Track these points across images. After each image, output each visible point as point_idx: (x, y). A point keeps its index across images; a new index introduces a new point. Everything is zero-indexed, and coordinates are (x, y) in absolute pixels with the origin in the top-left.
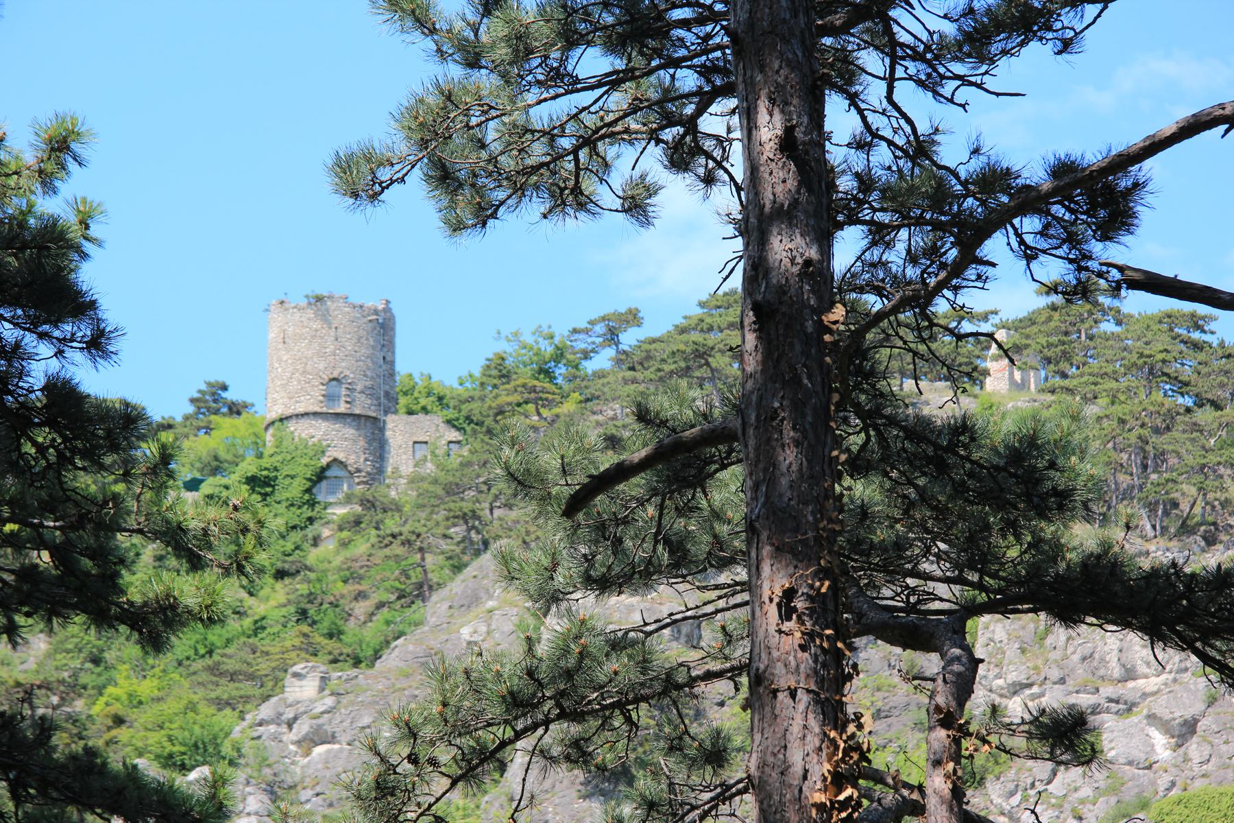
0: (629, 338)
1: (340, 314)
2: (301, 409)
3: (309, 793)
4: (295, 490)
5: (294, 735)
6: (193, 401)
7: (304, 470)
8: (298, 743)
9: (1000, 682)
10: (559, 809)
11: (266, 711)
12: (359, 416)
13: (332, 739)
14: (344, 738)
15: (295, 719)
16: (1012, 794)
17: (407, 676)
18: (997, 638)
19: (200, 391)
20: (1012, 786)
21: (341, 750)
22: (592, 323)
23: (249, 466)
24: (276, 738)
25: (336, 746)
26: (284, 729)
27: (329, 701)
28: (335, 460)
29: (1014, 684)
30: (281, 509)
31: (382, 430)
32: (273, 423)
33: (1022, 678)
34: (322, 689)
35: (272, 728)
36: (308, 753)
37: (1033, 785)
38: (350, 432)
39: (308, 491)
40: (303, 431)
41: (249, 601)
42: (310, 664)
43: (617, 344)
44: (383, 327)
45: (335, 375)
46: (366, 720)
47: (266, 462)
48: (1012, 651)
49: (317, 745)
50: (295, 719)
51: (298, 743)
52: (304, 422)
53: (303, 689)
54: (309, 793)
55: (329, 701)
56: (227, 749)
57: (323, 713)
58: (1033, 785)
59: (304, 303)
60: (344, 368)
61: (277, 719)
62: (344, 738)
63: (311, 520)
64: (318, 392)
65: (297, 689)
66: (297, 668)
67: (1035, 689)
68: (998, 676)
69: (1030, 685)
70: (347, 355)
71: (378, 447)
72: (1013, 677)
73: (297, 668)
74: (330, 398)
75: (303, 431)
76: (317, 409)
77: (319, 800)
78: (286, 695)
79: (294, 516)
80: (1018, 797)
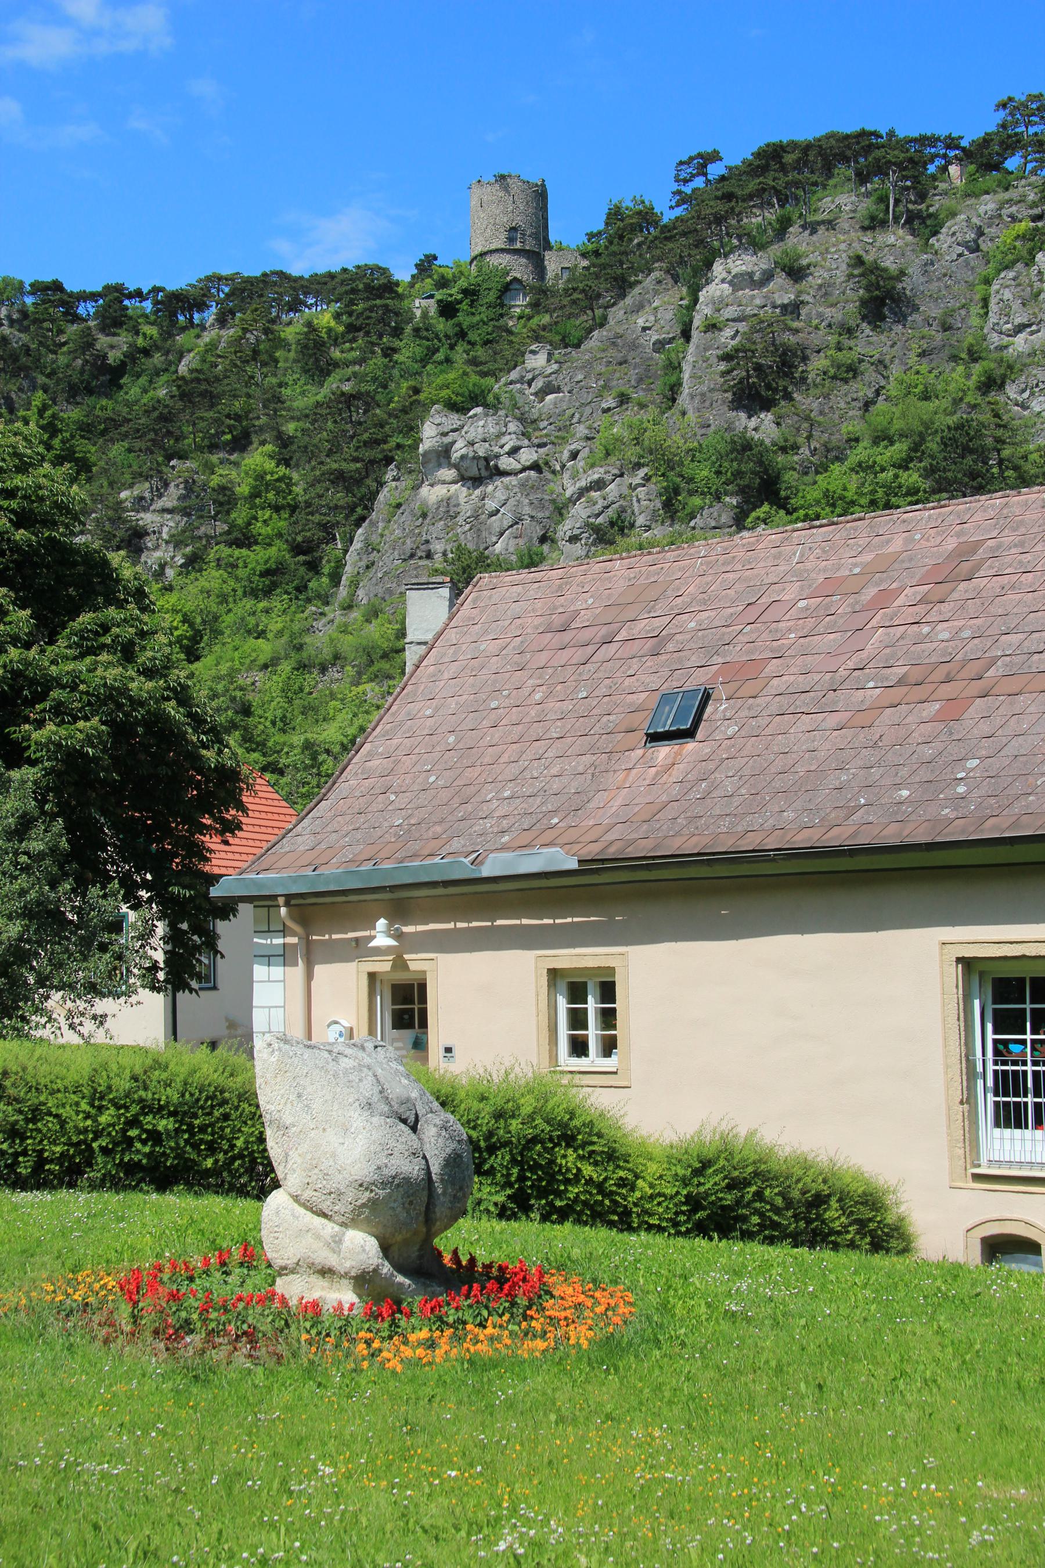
0: (715, 170)
1: (515, 186)
2: (493, 247)
3: (546, 423)
4: (492, 297)
5: (532, 390)
7: (495, 284)
8: (536, 394)
9: (1009, 326)
11: (514, 375)
13: (558, 390)
14: (566, 389)
15: (533, 379)
16: (1023, 391)
17: (604, 351)
18: (1005, 298)
20: (1023, 386)
22: (691, 159)
23: (463, 283)
24: (521, 392)
26: (526, 386)
27: (555, 367)
29: (1020, 325)
30: (483, 309)
31: (543, 260)
32: (475, 258)
33: (1025, 321)
34: (549, 361)
35: (518, 386)
36: (542, 400)
37: (1037, 385)
38: (523, 261)
39: (499, 297)
40: (494, 260)
41: (335, 635)
43: (705, 175)
44: (540, 196)
46: (580, 377)
47: (473, 281)
48: (1016, 305)
50: (533, 379)
51: (536, 394)
52: (497, 255)
53: (537, 361)
54: (546, 423)
55: (555, 367)
56: (490, 398)
58: (1037, 385)
59: (493, 180)
60: (518, 220)
61: (521, 380)
62: (566, 389)
63: (502, 316)
64: (503, 236)
67: (1034, 328)
68: (1007, 323)
69: (1030, 326)
70: (520, 215)
71: (540, 269)
72: (1018, 321)
73: (533, 347)
74: (511, 240)
75: (494, 260)
77: (552, 427)
79: (491, 313)
80: (1028, 392)
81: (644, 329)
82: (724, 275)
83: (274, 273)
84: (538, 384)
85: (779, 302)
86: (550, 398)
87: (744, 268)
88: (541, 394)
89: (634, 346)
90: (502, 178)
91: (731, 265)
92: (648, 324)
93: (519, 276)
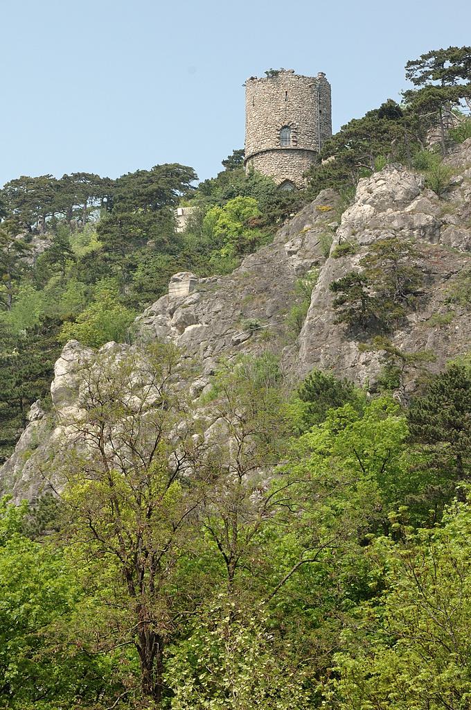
2: (264, 148)
5: (173, 321)
6: (224, 163)
10: (327, 351)
11: (156, 306)
12: (302, 150)
13: (197, 321)
15: (174, 309)
19: (229, 157)
21: (202, 328)
25: (200, 325)
27: (195, 296)
28: (287, 180)
34: (191, 289)
42: (184, 273)
45: (286, 123)
49: (187, 325)
50: (174, 309)
57: (190, 304)
60: (293, 119)
62: (204, 319)
65: (176, 290)
66: (175, 276)
76: (275, 147)
78: (170, 294)
81: (291, 253)
82: (366, 195)
83: (77, 176)
84: (178, 315)
85: (416, 224)
86: (189, 329)
87: (384, 188)
88: (181, 326)
89: (280, 272)
90: (274, 74)
91: (373, 186)
92: (294, 249)
93: (291, 178)
